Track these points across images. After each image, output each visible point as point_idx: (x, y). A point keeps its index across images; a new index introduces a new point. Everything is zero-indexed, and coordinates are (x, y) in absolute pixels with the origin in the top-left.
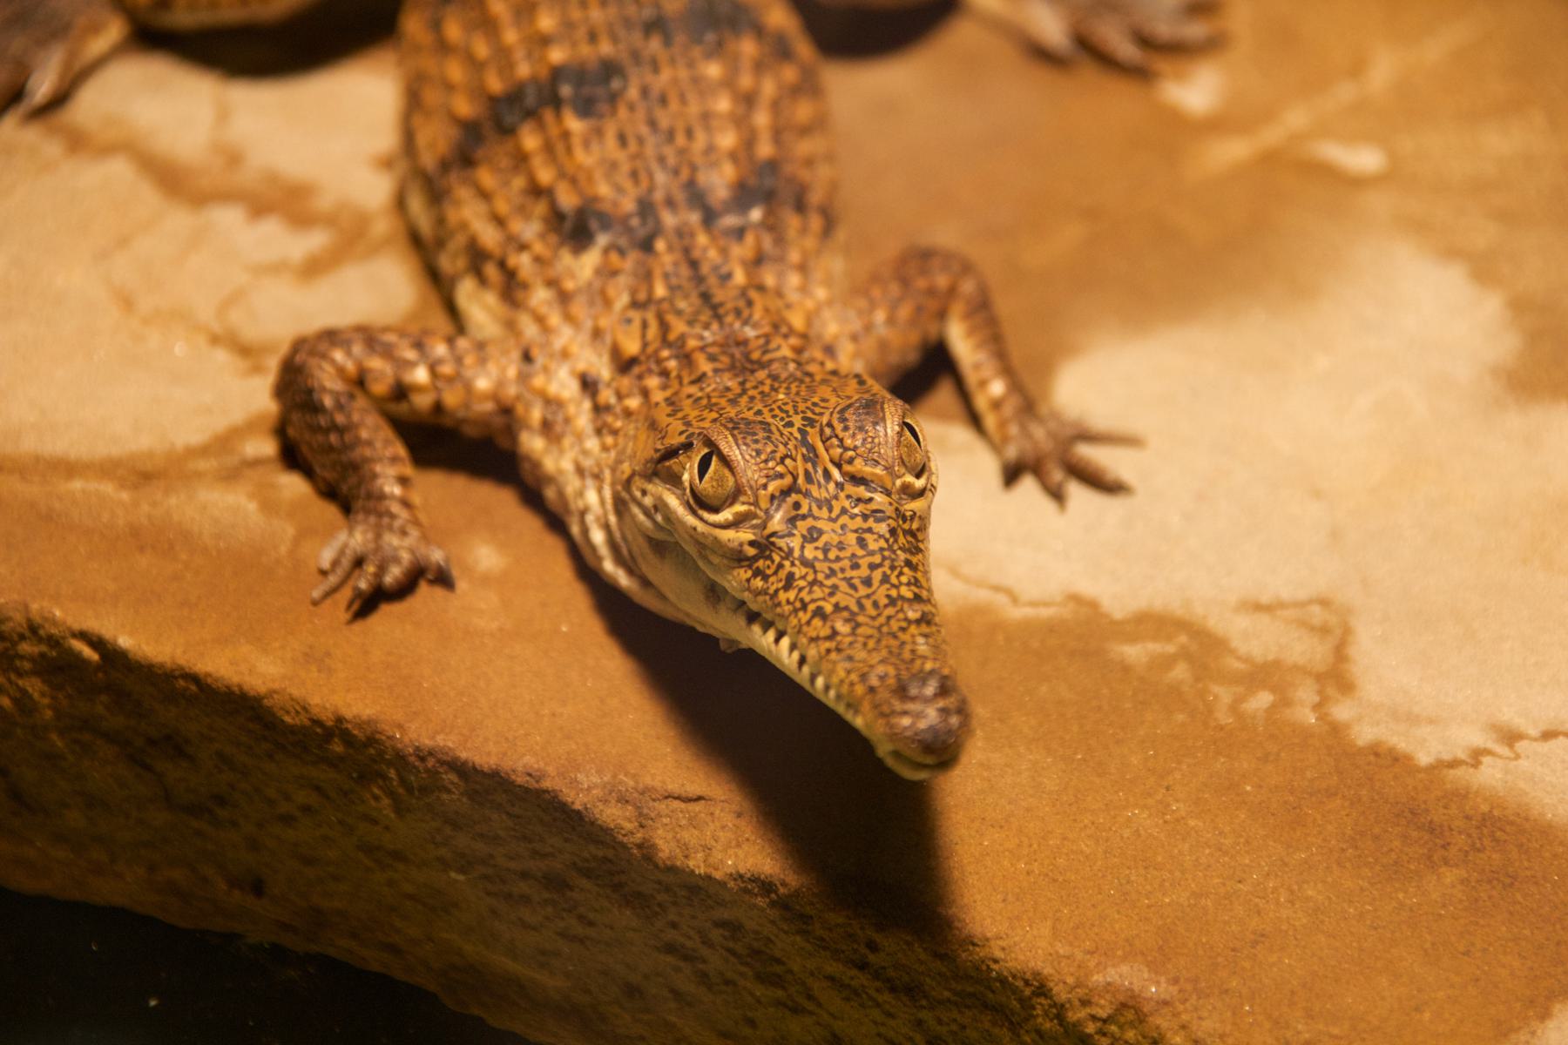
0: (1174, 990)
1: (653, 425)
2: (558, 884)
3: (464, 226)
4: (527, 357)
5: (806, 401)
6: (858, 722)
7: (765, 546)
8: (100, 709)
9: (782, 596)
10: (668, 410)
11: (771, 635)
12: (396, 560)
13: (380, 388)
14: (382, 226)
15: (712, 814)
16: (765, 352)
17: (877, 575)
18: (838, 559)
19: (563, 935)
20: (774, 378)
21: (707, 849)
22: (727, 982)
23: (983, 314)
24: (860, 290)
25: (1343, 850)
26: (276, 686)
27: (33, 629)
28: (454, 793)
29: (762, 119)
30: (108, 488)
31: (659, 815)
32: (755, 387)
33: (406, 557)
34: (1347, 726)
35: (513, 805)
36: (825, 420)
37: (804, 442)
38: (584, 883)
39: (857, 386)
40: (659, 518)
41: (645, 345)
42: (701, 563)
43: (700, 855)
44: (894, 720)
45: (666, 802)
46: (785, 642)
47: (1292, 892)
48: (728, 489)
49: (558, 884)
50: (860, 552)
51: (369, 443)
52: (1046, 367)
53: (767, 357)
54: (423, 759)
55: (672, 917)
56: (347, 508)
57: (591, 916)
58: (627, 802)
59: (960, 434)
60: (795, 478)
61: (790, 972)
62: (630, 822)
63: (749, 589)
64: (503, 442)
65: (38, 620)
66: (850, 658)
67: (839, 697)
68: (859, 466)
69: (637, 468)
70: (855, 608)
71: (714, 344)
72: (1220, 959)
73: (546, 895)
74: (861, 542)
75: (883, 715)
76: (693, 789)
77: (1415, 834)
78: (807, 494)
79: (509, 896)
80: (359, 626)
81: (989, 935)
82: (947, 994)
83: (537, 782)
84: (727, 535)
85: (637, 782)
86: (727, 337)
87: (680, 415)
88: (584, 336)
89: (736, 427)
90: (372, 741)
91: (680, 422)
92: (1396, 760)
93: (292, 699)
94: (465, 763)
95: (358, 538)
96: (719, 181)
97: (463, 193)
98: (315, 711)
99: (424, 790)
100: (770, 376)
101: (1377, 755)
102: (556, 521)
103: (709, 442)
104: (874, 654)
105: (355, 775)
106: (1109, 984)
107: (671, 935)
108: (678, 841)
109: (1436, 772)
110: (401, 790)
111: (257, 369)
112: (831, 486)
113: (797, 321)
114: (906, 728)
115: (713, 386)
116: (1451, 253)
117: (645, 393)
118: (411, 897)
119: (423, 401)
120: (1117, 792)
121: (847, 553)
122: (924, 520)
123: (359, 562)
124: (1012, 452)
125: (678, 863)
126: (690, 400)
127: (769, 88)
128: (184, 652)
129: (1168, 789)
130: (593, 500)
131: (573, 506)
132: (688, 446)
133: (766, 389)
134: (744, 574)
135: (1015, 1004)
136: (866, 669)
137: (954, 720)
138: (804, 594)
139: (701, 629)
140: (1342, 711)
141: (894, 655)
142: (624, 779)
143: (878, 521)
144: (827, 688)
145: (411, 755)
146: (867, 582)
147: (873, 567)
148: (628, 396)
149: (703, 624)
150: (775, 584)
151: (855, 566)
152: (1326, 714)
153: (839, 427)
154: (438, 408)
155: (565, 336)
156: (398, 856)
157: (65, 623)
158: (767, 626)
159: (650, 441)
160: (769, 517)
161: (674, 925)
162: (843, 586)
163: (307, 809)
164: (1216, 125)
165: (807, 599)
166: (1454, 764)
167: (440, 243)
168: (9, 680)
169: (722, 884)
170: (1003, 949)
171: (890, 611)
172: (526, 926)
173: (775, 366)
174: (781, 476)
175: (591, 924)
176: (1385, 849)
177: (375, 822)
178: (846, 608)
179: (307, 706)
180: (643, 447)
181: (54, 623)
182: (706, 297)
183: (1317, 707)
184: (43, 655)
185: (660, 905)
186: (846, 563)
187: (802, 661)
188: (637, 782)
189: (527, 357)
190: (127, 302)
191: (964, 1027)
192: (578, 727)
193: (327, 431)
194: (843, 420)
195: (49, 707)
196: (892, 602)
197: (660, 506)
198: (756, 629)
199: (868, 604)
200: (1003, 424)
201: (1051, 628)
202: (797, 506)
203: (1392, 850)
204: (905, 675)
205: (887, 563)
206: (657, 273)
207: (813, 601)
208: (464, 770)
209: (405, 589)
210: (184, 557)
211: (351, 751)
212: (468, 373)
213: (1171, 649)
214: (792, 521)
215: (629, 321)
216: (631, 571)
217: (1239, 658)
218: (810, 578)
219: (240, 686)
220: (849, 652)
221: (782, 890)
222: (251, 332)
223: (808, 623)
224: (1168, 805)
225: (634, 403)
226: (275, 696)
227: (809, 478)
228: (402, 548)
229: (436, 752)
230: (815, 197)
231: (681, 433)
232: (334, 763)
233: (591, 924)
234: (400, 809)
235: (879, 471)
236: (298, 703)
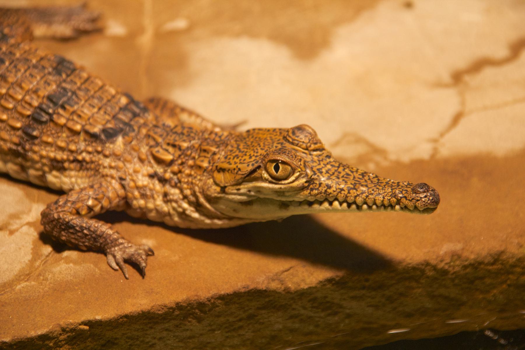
7: (310, 181)
21: (303, 280)
27: (64, 330)
28: (220, 306)
30: (23, 284)
38: (263, 312)
48: (289, 171)
54: (209, 301)
58: (275, 280)
63: (311, 195)
65: (64, 326)
80: (145, 277)
83: (248, 288)
84: (296, 184)
93: (160, 306)
98: (169, 305)
119: (97, 209)
145: (206, 302)
154: (102, 208)
157: (75, 322)
170: (411, 259)
179: (166, 305)
181: (72, 324)
184: (68, 337)
208: (222, 298)
211: (182, 311)
219: (142, 311)
221: (337, 279)
226: (154, 307)
229: (213, 297)
236: (163, 306)
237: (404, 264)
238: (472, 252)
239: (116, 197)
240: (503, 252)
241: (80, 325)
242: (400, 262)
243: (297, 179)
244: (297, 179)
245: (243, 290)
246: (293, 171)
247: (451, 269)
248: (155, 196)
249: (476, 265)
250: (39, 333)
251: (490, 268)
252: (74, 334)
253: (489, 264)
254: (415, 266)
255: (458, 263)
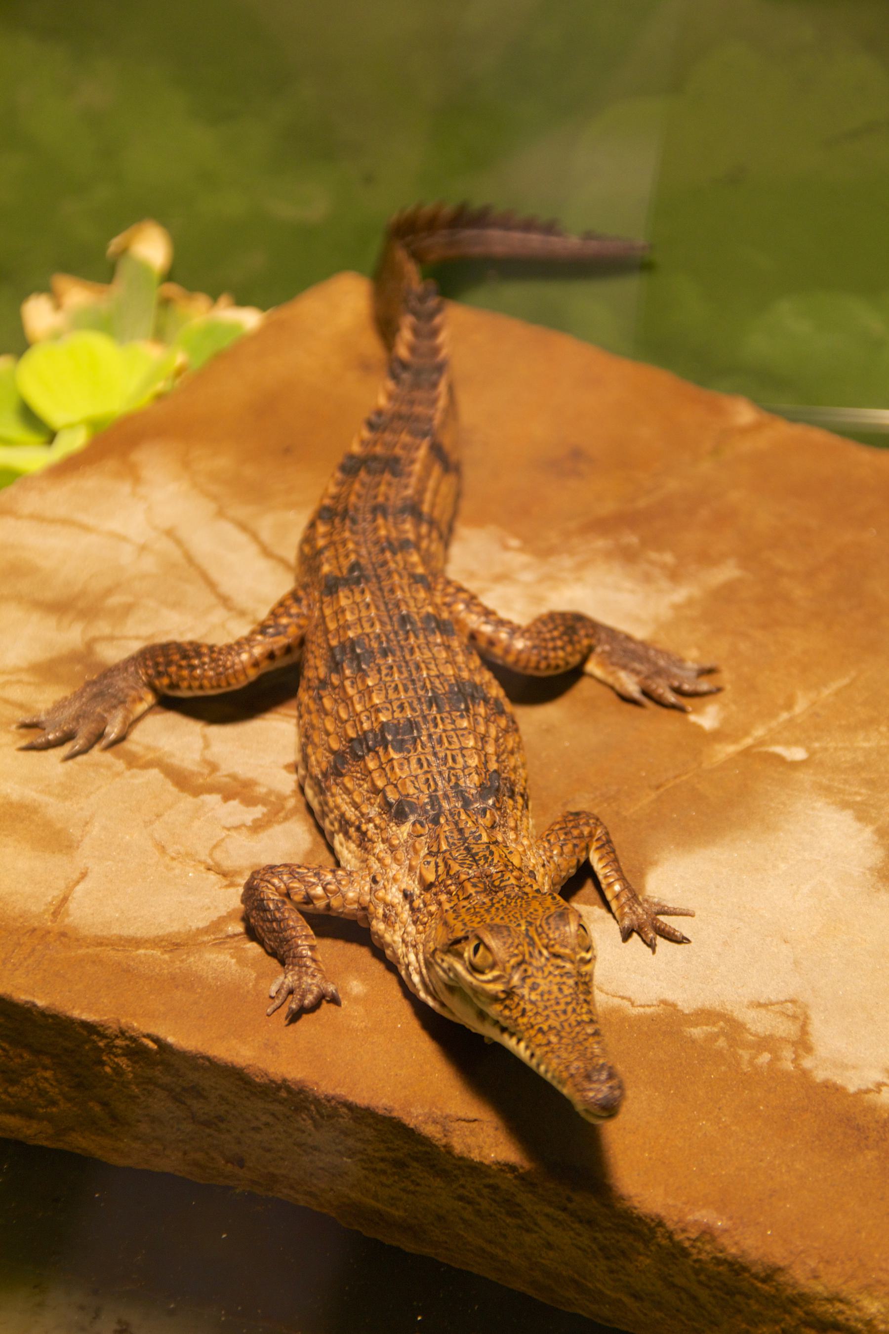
0: (730, 1223)
1: (446, 924)
2: (400, 1164)
3: (338, 807)
4: (374, 881)
5: (526, 911)
6: (565, 1091)
7: (510, 993)
8: (157, 1073)
9: (520, 1021)
10: (454, 916)
11: (514, 1041)
12: (311, 992)
13: (297, 898)
14: (291, 803)
15: (482, 1129)
16: (502, 881)
17: (570, 1008)
18: (548, 1000)
19: (404, 1190)
20: (508, 896)
21: (480, 1148)
22: (491, 1215)
23: (607, 844)
24: (544, 837)
25: (813, 1142)
26: (251, 1062)
27: (123, 1033)
29: (491, 749)
30: (157, 953)
31: (454, 1130)
32: (498, 902)
33: (315, 989)
34: (811, 1071)
35: (377, 1124)
36: (538, 923)
37: (527, 935)
38: (415, 1164)
39: (551, 901)
40: (451, 975)
41: (438, 876)
42: (475, 1000)
43: (477, 1151)
44: (585, 1094)
45: (457, 1123)
46: (522, 1045)
47: (788, 1166)
49: (400, 1164)
50: (560, 996)
51: (294, 928)
52: (641, 874)
53: (503, 884)
54: (329, 1101)
55: (462, 1182)
56: (283, 963)
57: (418, 1180)
58: (437, 1123)
59: (599, 911)
60: (524, 956)
61: (525, 1210)
62: (439, 1133)
63: (501, 1015)
64: (363, 925)
65: (125, 1028)
66: (559, 1057)
67: (553, 1077)
68: (558, 949)
69: (438, 947)
70: (559, 1027)
71: (475, 876)
72: (753, 1206)
73: (394, 1170)
74: (560, 990)
75: (579, 1091)
76: (472, 1115)
77: (850, 1132)
78: (530, 964)
79: (374, 1170)
80: (291, 1027)
81: (632, 1194)
82: (609, 1224)
83: (390, 1113)
85: (442, 1112)
86: (481, 873)
87: (460, 919)
88: (405, 870)
89: (495, 929)
90: (301, 1091)
91: (461, 923)
92: (837, 1090)
94: (351, 1103)
95: (290, 979)
96: (471, 783)
97: (336, 790)
98: (272, 1076)
99: (330, 1117)
100: (505, 895)
101: (827, 1087)
102: (392, 967)
103: (478, 937)
104: (572, 1055)
105: (293, 1108)
106: (696, 1221)
107: (461, 1191)
108: (465, 1144)
109: (858, 1096)
110: (318, 1117)
111: (232, 885)
112: (543, 960)
113: (516, 861)
114: (593, 1097)
115: (476, 901)
116: (845, 805)
117: (440, 904)
118: (322, 1169)
119: (320, 904)
120: (693, 1112)
121: (553, 997)
122: (590, 975)
123: (291, 992)
124: (627, 922)
125: (465, 1155)
126: (464, 910)
127: (493, 732)
128: (202, 1045)
129: (719, 1109)
130: (412, 959)
131: (401, 960)
132: (466, 938)
133: (504, 903)
134: (498, 1007)
135: (646, 1231)
136: (568, 1064)
137: (617, 1093)
138: (532, 1020)
139: (473, 1031)
140: (807, 1063)
141: (582, 1056)
142: (436, 1111)
143: (569, 978)
144: (547, 1071)
146: (565, 1012)
147: (567, 1004)
148: (430, 905)
149: (474, 1028)
150: (516, 1013)
151: (558, 1003)
152: (799, 1065)
153: (546, 927)
154: (328, 907)
155: (394, 869)
156: (315, 1148)
157: (139, 1030)
158: (512, 1035)
159: (445, 932)
160: (511, 978)
161: (463, 1186)
162: (552, 1015)
163: (267, 1124)
164: (717, 736)
165: (534, 1022)
166: (868, 1091)
167: (324, 815)
168: (110, 1058)
169: (489, 1167)
170: (639, 1202)
171: (578, 1029)
172: (383, 1185)
173: (508, 889)
174: (516, 955)
175: (418, 1185)
176: (835, 1141)
177: (303, 1132)
178: (555, 1028)
180: (439, 936)
181: (134, 1029)
182: (468, 849)
183: (794, 1061)
184: (127, 1046)
185: (455, 1176)
186: (553, 1002)
187: (532, 1055)
188: (442, 1112)
189: (374, 881)
190: (163, 849)
191: (618, 1241)
192: (409, 1081)
193: (271, 922)
194: (548, 924)
195: (131, 1072)
196: (579, 1023)
197: (451, 968)
198: (506, 1036)
199: (566, 1025)
200: (621, 907)
201: (652, 1019)
202: (526, 971)
203: (838, 1141)
204: (590, 1068)
205: (574, 1002)
206: (442, 836)
207: (537, 1024)
208: (351, 1107)
209: (314, 1007)
210: (199, 990)
212: (343, 889)
213: (716, 1029)
214: (523, 979)
215: (429, 863)
216: (434, 998)
217: (751, 1034)
218: (535, 1011)
219: (232, 1063)
220: (557, 1053)
221: (521, 1171)
222: (227, 864)
223: (535, 1036)
224: (720, 1118)
225: (433, 908)
227: (531, 955)
228: (313, 984)
230: (518, 789)
231: (462, 930)
232: (282, 1102)
233: (418, 1185)
234: (317, 1126)
235: (567, 951)
237: (628, 1204)
238: (736, 1243)
239: (355, 902)
240: (780, 1269)
241: (144, 1036)
242: (621, 1198)
243: (495, 980)
244: (495, 980)
245: (381, 1112)
246: (493, 967)
247: (694, 1251)
248: (397, 926)
249: (737, 1268)
250: (85, 1017)
251: (759, 1285)
252: (134, 1045)
253: (756, 1276)
254: (641, 1215)
255: (708, 1247)
